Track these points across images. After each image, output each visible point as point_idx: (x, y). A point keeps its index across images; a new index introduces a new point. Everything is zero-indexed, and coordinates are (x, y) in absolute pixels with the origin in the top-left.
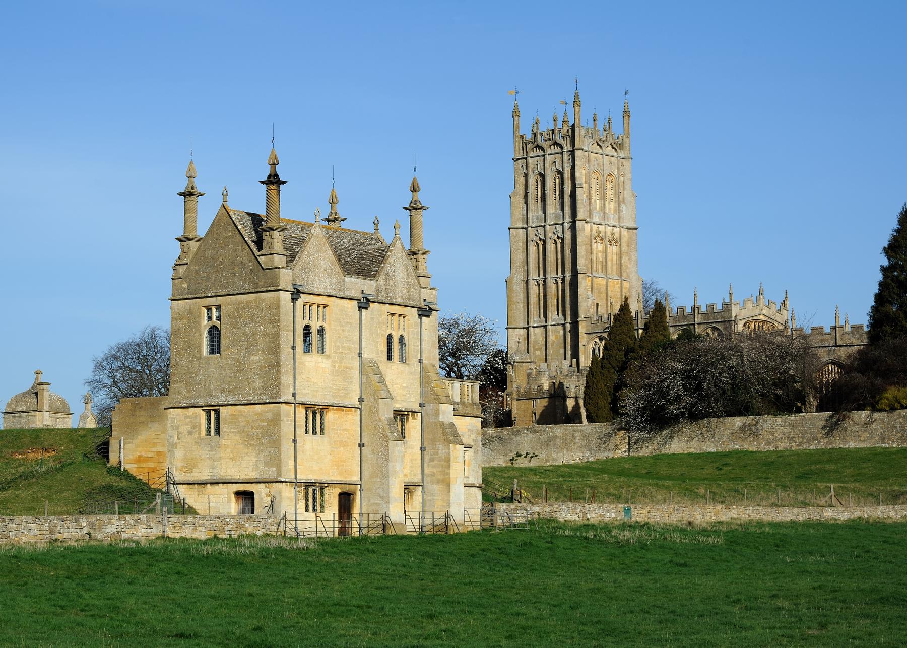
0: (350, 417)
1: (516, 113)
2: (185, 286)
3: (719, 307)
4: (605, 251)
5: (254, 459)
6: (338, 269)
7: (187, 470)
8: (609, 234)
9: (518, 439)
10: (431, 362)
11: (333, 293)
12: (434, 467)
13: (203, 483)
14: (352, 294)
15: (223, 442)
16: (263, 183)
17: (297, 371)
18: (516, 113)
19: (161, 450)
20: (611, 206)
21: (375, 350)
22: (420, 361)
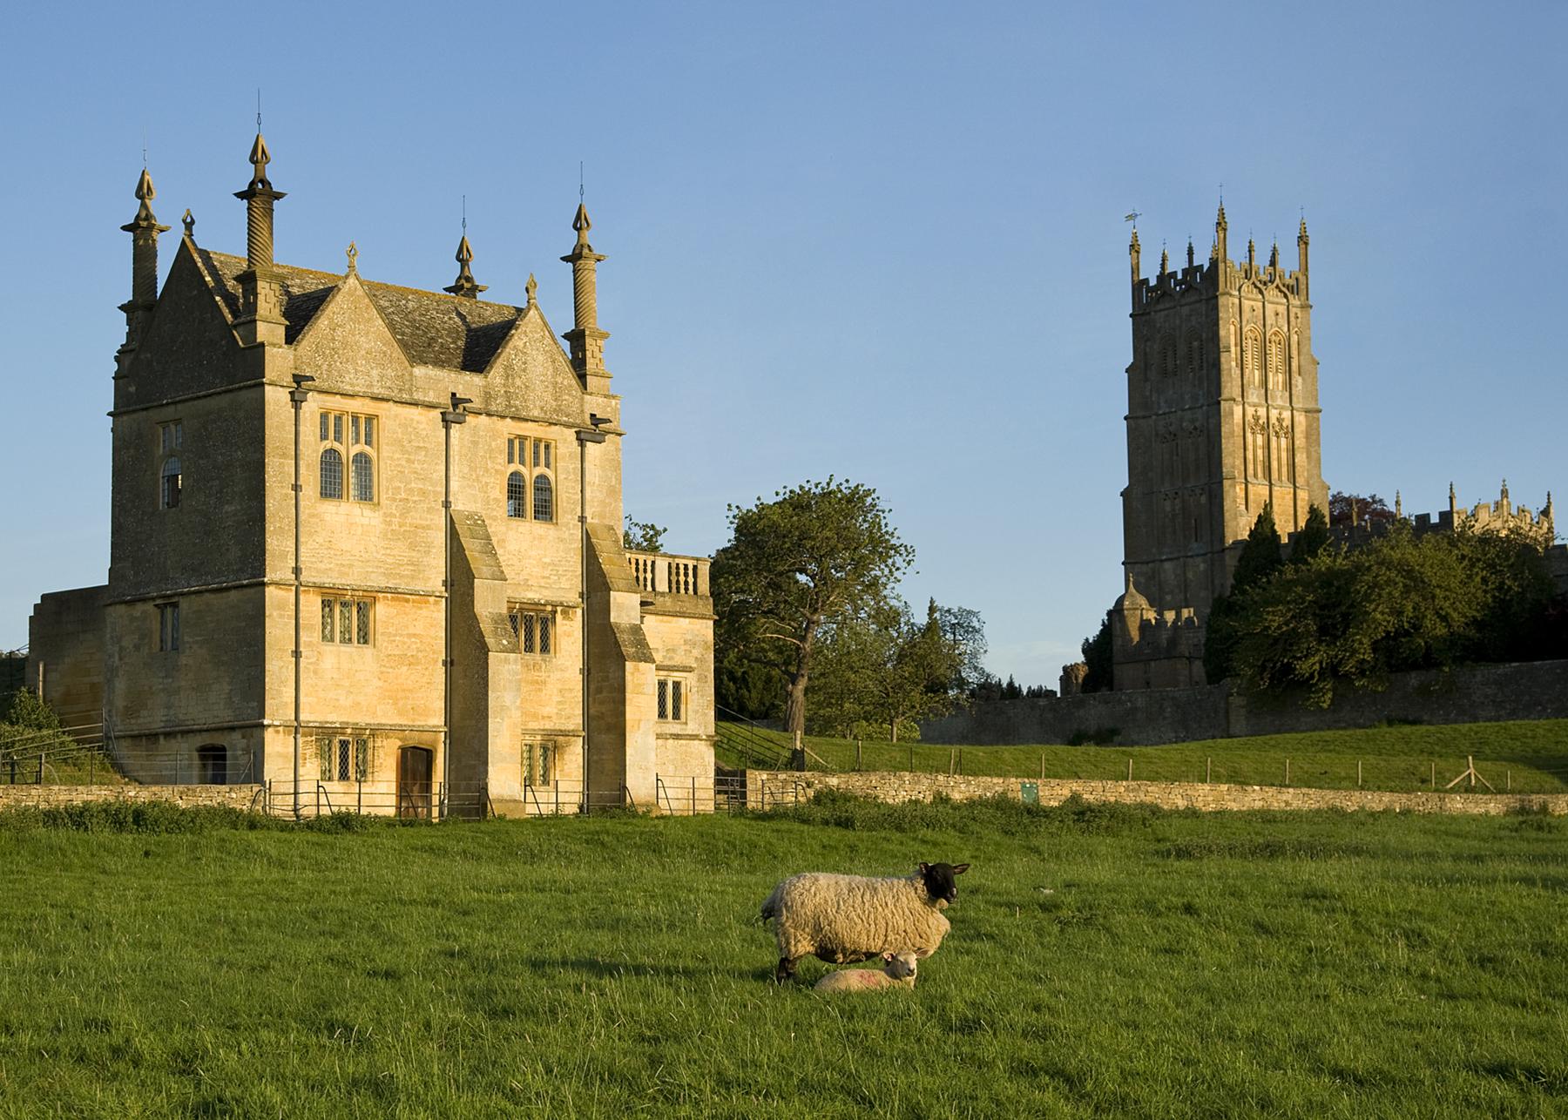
0: (424, 612)
1: (1134, 248)
2: (132, 389)
3: (1435, 519)
4: (1268, 446)
5: (227, 688)
6: (397, 352)
7: (131, 712)
8: (1273, 420)
9: (1082, 712)
10: (607, 522)
11: (384, 393)
12: (602, 703)
13: (152, 737)
14: (431, 397)
15: (183, 660)
16: (240, 195)
17: (301, 529)
18: (1134, 248)
19: (95, 679)
20: (1276, 380)
21: (480, 495)
22: (582, 519)
